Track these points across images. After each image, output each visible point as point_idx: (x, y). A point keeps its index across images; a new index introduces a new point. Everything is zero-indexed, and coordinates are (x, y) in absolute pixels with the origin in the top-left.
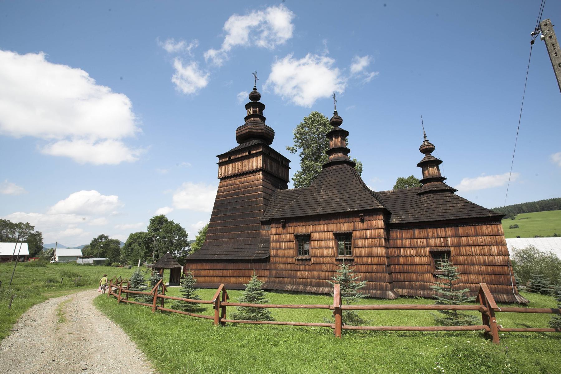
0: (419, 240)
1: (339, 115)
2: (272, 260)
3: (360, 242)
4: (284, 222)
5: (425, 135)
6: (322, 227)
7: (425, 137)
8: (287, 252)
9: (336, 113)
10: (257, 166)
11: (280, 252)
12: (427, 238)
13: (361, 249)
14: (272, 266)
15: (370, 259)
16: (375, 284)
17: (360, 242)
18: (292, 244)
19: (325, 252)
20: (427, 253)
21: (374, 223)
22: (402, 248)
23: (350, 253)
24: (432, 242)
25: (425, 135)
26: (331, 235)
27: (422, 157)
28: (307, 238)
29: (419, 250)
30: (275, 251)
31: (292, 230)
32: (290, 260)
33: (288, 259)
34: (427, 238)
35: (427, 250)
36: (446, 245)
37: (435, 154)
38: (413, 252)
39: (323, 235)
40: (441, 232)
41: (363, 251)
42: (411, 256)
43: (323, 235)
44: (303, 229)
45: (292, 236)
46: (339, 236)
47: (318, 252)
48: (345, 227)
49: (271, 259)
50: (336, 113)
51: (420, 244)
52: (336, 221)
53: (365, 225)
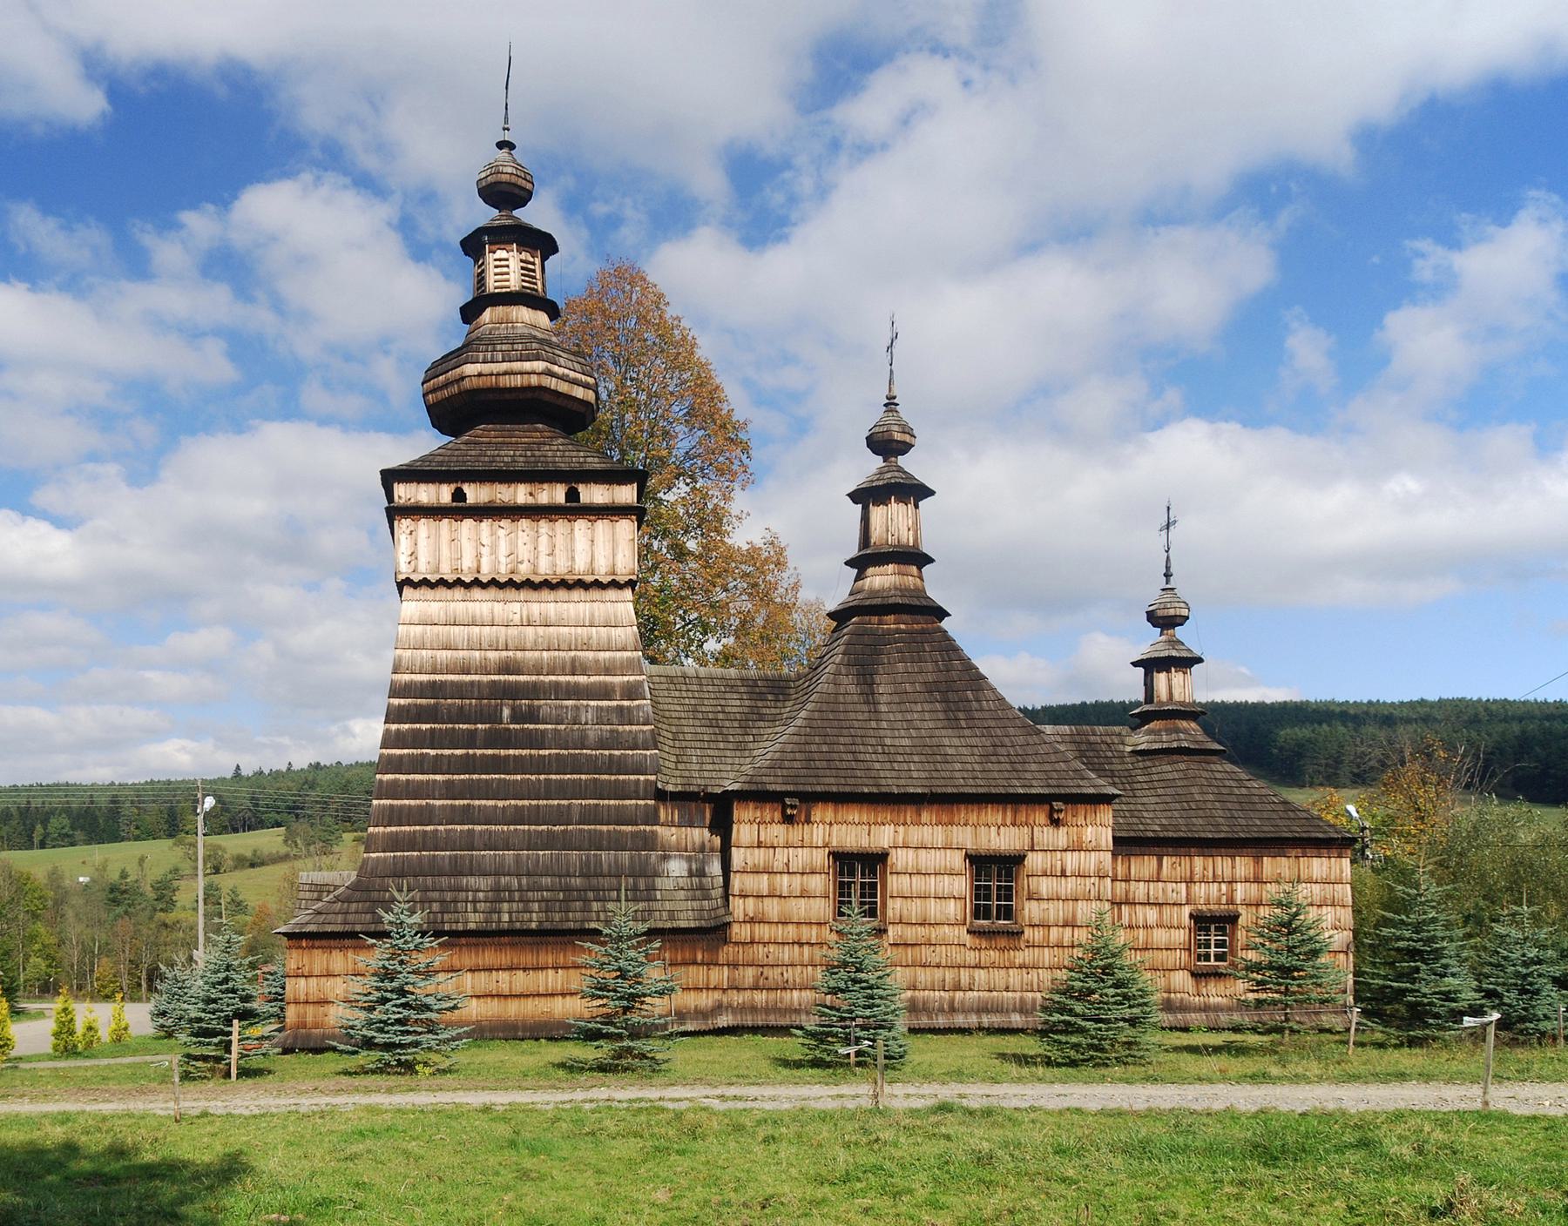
0: (1170, 886)
1: (905, 411)
2: (739, 932)
3: (1045, 886)
4: (791, 802)
5: (1168, 568)
6: (917, 834)
7: (1168, 575)
8: (800, 908)
9: (891, 404)
10: (496, 561)
11: (772, 908)
12: (1190, 881)
13: (1044, 905)
14: (741, 954)
15: (1068, 930)
16: (1021, 998)
17: (1045, 886)
18: (817, 883)
19: (933, 909)
20: (1186, 920)
21: (1089, 833)
22: (1127, 903)
23: (1007, 913)
24: (1200, 891)
25: (1168, 568)
26: (957, 860)
27: (1149, 641)
28: (875, 861)
29: (1167, 910)
30: (750, 901)
31: (818, 833)
32: (812, 934)
33: (804, 929)
34: (1190, 881)
35: (1187, 910)
36: (1231, 901)
37: (911, 464)
38: (1152, 915)
39: (929, 860)
40: (1223, 865)
41: (1055, 911)
42: (1146, 927)
43: (929, 860)
44: (999, 835)
45: (820, 858)
46: (844, 861)
47: (914, 909)
48: (999, 835)
49: (736, 928)
50: (891, 404)
51: (1172, 897)
52: (973, 818)
53: (1061, 837)
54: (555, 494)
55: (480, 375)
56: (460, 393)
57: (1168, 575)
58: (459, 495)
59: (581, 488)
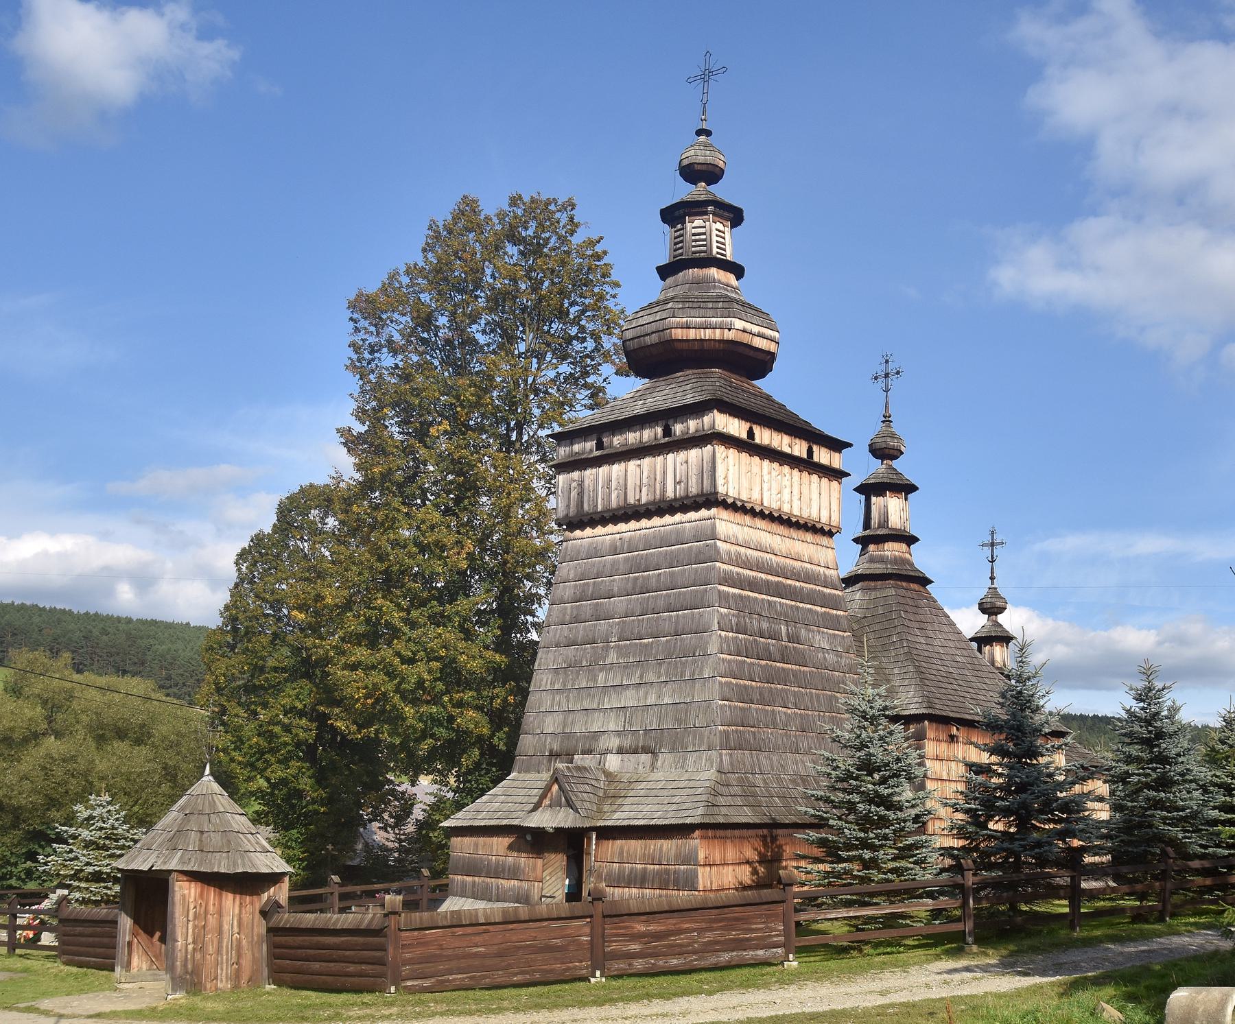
1: (895, 428)
5: (992, 572)
7: (992, 578)
9: (887, 420)
25: (992, 572)
37: (904, 467)
50: (887, 420)
54: (798, 448)
55: (744, 331)
56: (721, 341)
57: (992, 578)
58: (751, 434)
59: (744, 436)
